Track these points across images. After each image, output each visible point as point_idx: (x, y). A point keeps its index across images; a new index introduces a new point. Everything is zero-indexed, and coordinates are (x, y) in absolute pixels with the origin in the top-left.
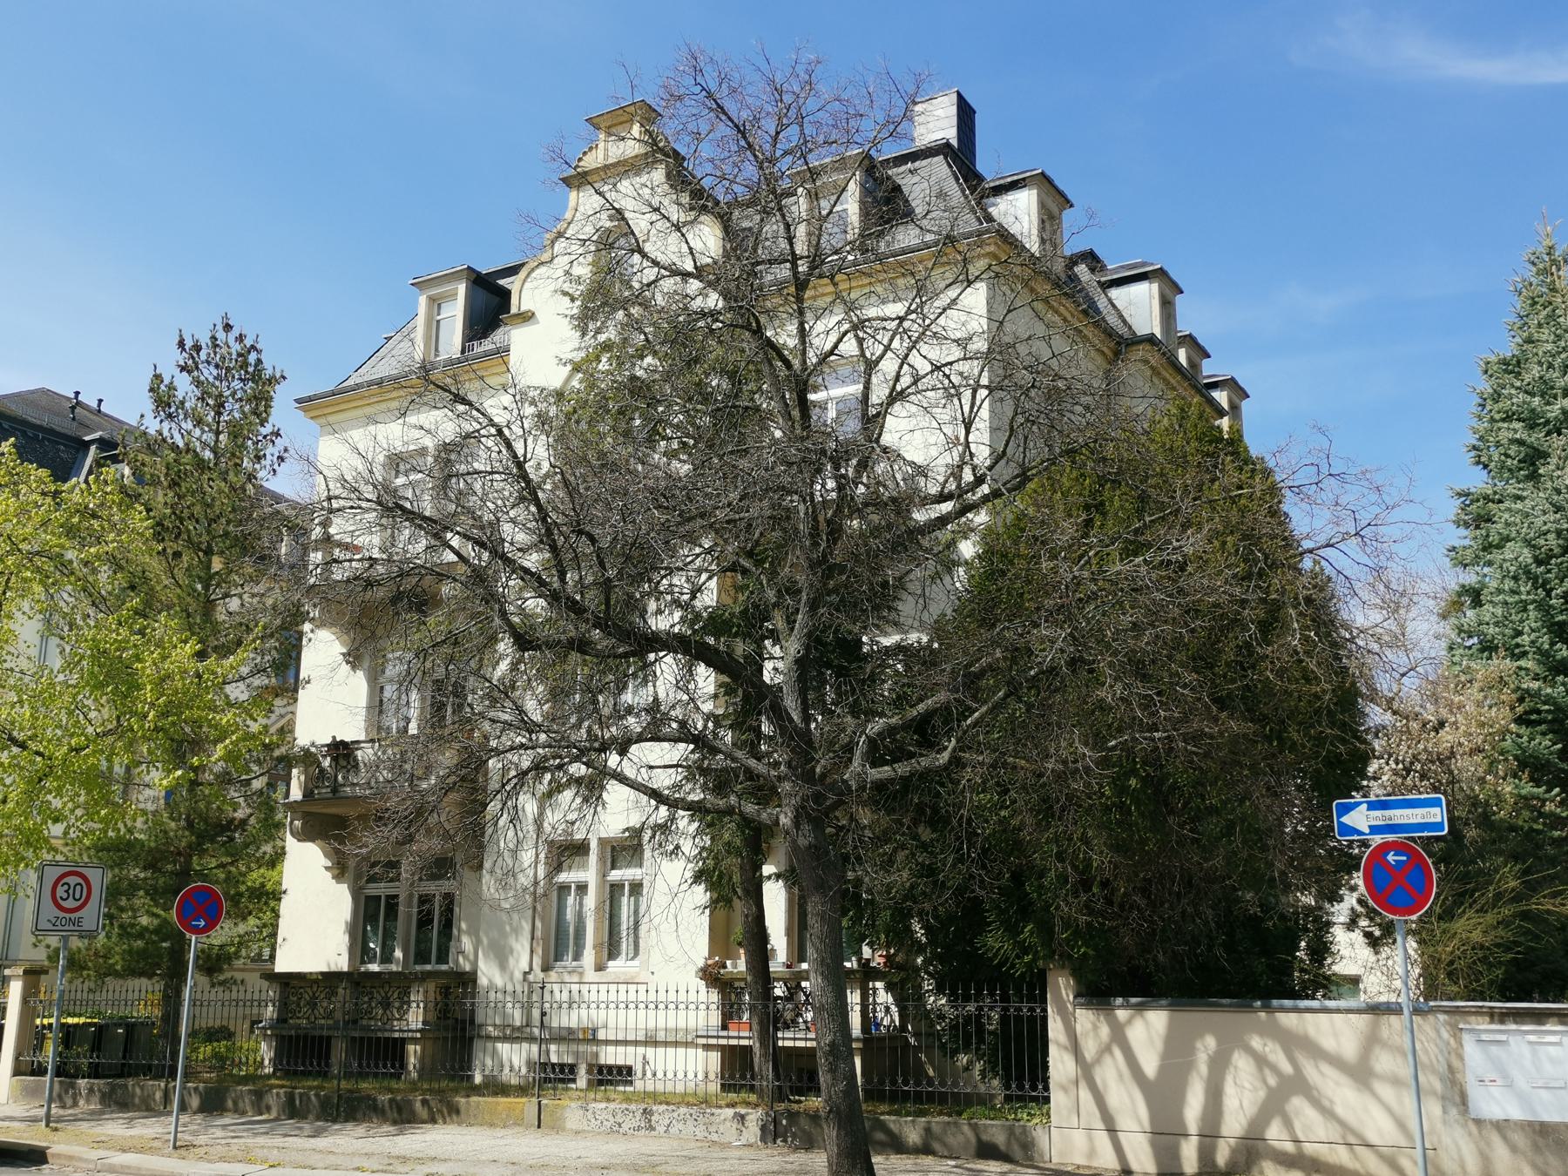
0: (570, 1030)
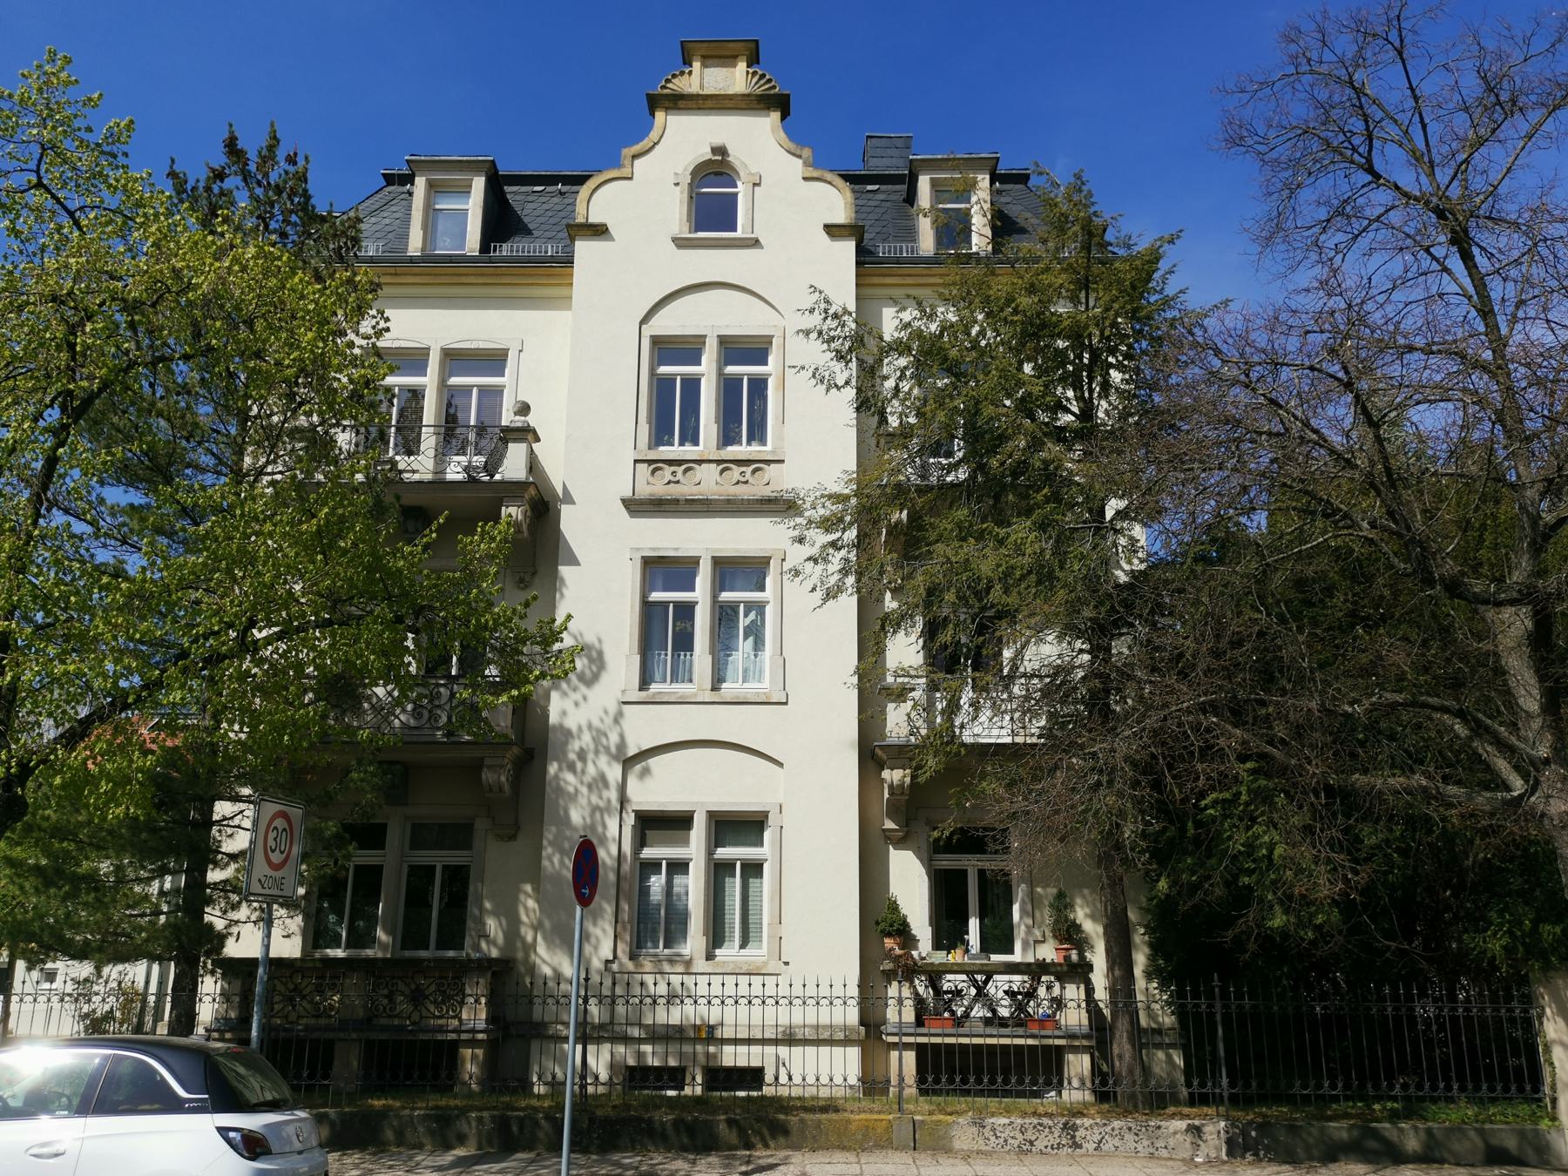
0: (680, 1029)
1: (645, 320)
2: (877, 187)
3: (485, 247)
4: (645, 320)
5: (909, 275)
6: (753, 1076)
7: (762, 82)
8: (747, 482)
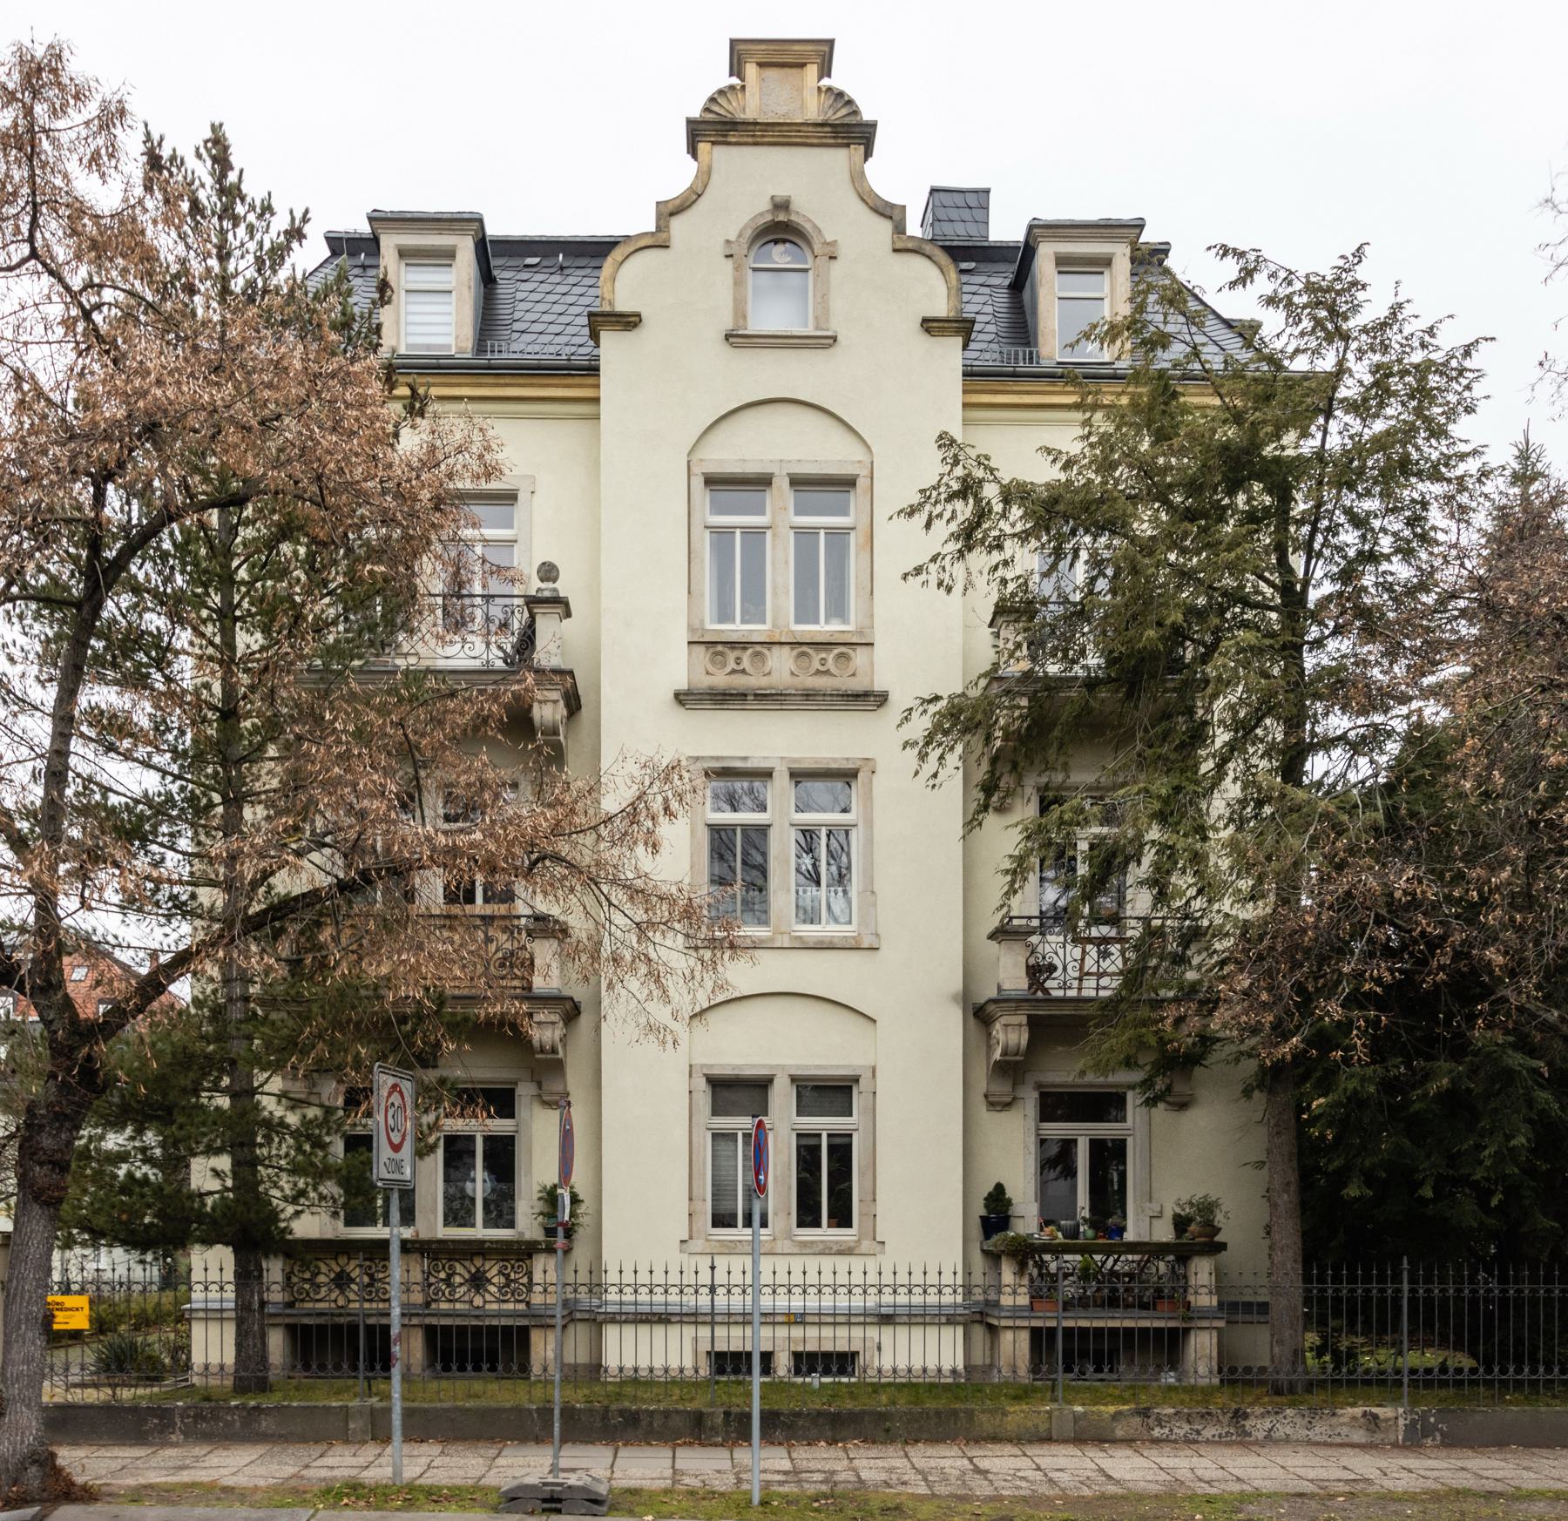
2: (972, 265)
5: (1028, 393)
6: (843, 1362)
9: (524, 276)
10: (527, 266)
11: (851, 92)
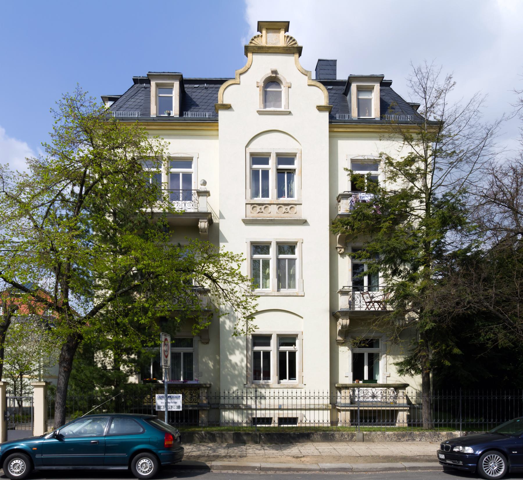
1: (247, 146)
3: (181, 114)
4: (247, 146)
6: (294, 420)
7: (291, 41)
8: (288, 212)
9: (194, 90)
10: (195, 87)
11: (294, 37)
